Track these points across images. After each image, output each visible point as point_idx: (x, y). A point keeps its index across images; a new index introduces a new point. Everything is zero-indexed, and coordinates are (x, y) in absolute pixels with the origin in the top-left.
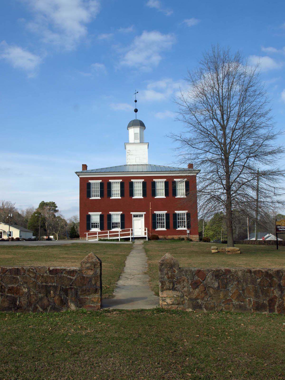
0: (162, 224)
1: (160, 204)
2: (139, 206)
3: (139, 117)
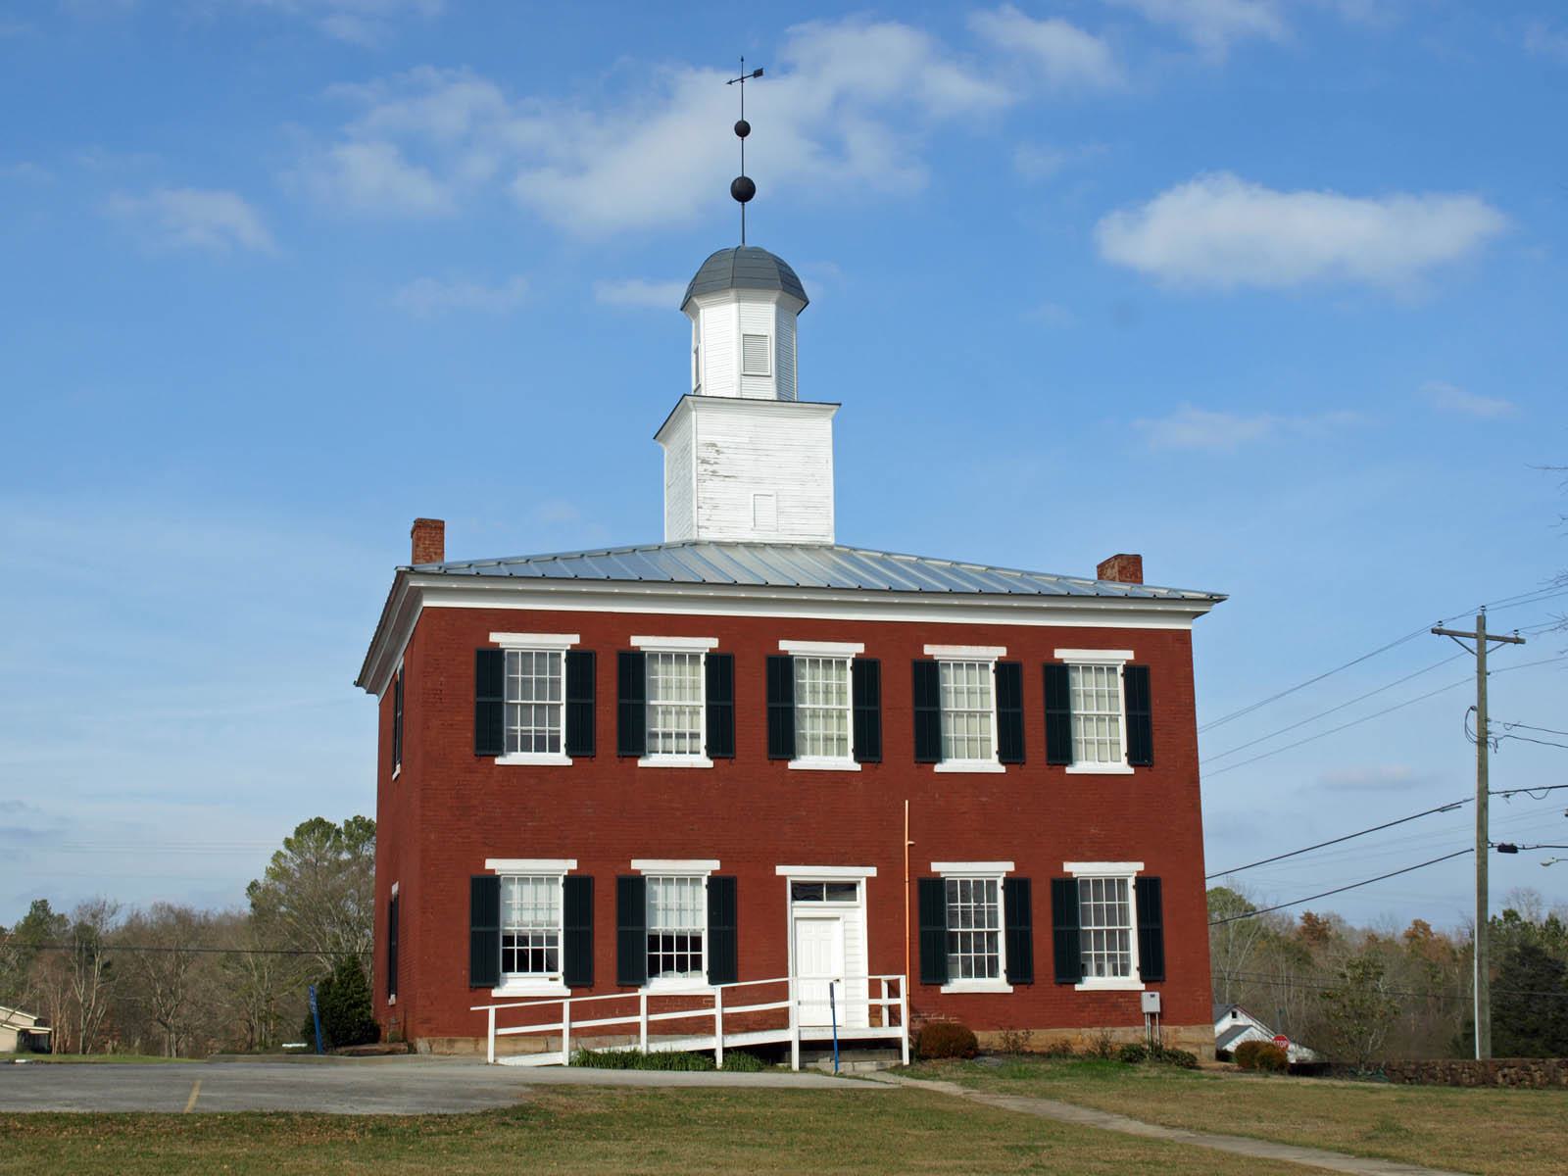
0: (979, 948)
1: (970, 816)
2: (830, 820)
3: (762, 230)
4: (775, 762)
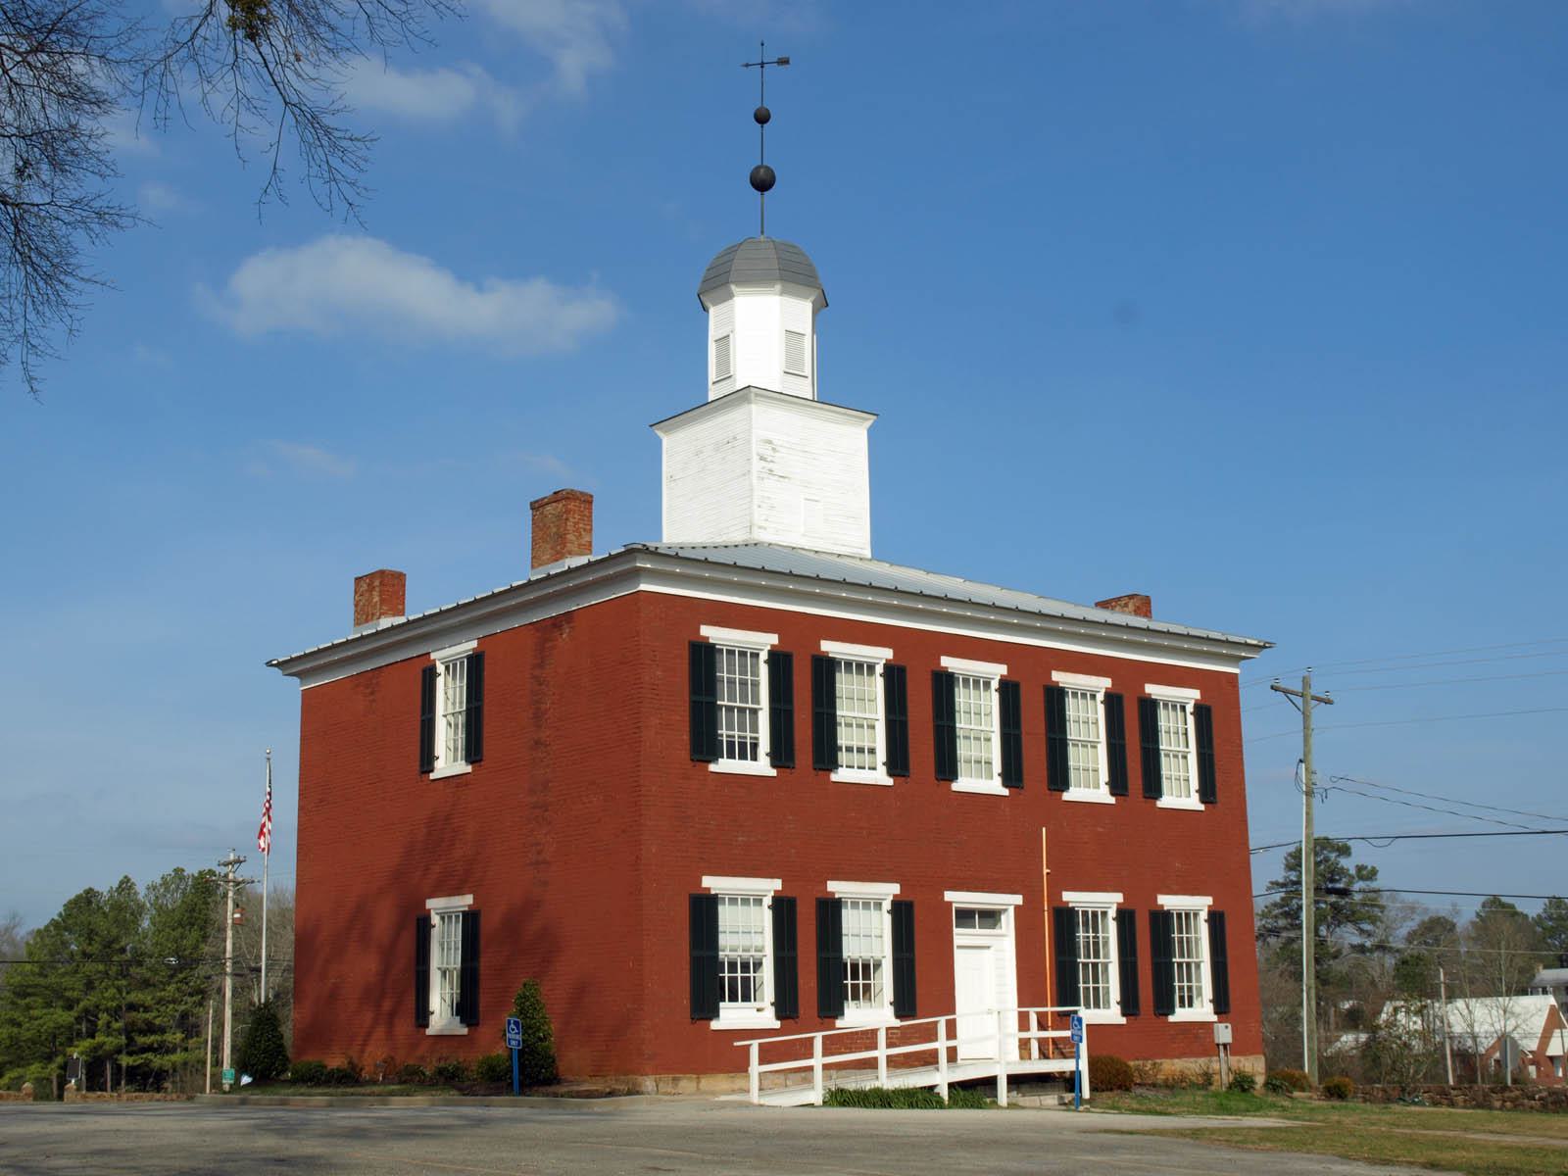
2: (987, 845)
4: (820, 772)
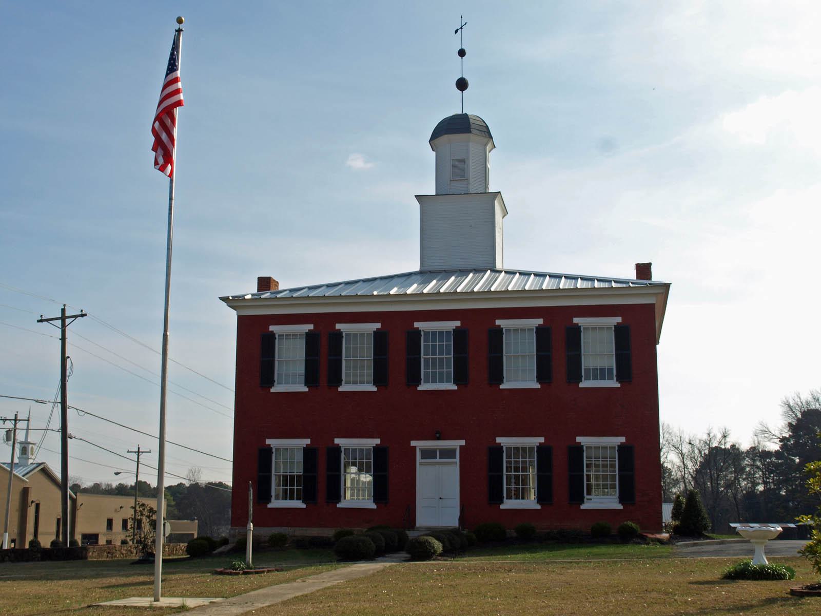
1: (521, 412)
2: (439, 417)
